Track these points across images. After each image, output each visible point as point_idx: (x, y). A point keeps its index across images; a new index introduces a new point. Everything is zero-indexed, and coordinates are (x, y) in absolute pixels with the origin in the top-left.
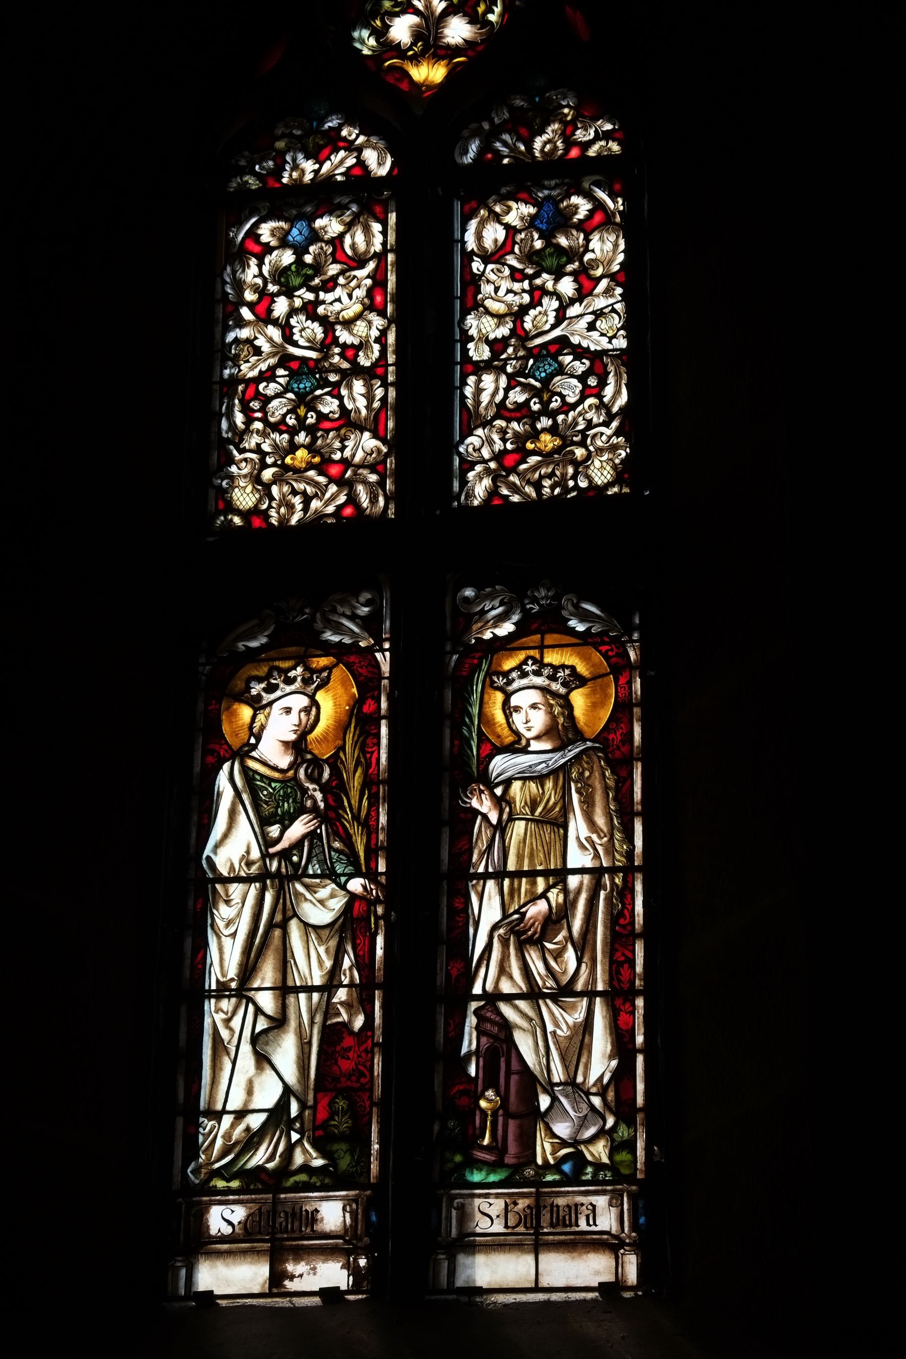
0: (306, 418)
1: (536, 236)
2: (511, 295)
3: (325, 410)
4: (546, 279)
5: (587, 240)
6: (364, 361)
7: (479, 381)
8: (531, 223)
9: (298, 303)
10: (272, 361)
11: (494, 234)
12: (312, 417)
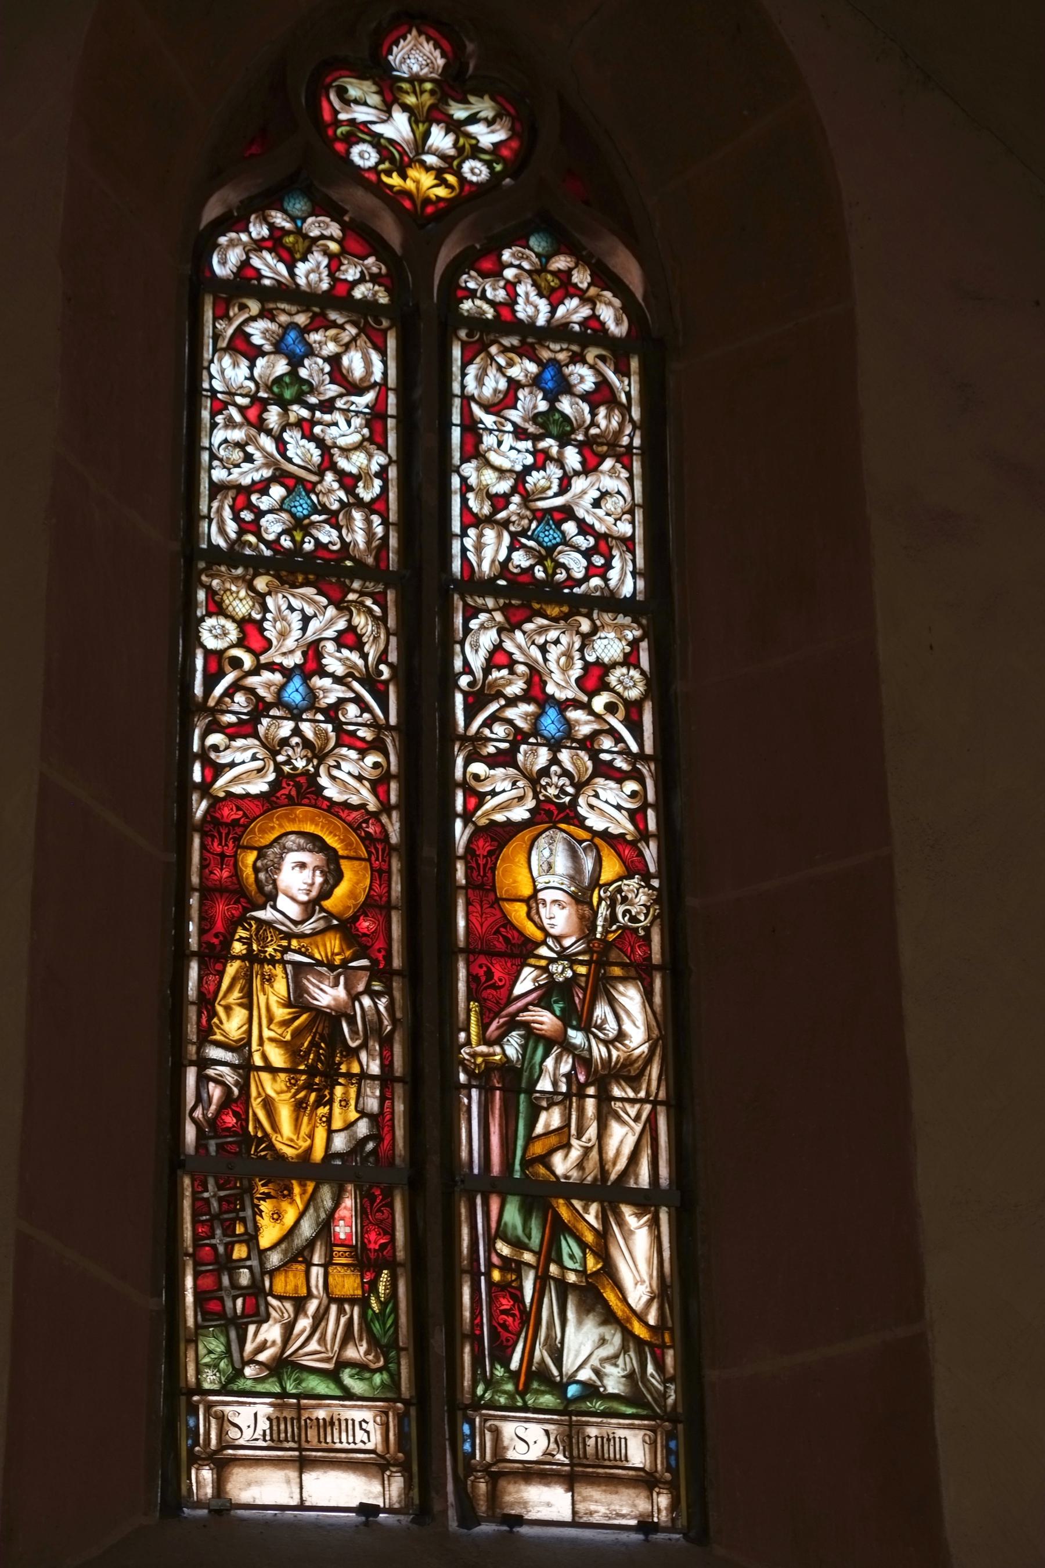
0: (303, 542)
1: (540, 396)
2: (514, 452)
3: (324, 539)
4: (549, 444)
5: (593, 414)
6: (367, 496)
7: (481, 535)
8: (536, 382)
9: (292, 418)
10: (267, 473)
11: (494, 384)
12: (310, 542)
